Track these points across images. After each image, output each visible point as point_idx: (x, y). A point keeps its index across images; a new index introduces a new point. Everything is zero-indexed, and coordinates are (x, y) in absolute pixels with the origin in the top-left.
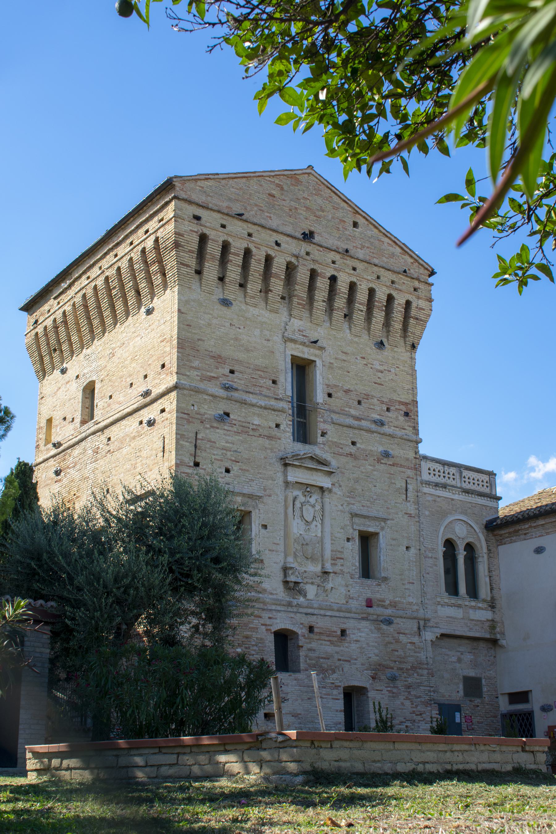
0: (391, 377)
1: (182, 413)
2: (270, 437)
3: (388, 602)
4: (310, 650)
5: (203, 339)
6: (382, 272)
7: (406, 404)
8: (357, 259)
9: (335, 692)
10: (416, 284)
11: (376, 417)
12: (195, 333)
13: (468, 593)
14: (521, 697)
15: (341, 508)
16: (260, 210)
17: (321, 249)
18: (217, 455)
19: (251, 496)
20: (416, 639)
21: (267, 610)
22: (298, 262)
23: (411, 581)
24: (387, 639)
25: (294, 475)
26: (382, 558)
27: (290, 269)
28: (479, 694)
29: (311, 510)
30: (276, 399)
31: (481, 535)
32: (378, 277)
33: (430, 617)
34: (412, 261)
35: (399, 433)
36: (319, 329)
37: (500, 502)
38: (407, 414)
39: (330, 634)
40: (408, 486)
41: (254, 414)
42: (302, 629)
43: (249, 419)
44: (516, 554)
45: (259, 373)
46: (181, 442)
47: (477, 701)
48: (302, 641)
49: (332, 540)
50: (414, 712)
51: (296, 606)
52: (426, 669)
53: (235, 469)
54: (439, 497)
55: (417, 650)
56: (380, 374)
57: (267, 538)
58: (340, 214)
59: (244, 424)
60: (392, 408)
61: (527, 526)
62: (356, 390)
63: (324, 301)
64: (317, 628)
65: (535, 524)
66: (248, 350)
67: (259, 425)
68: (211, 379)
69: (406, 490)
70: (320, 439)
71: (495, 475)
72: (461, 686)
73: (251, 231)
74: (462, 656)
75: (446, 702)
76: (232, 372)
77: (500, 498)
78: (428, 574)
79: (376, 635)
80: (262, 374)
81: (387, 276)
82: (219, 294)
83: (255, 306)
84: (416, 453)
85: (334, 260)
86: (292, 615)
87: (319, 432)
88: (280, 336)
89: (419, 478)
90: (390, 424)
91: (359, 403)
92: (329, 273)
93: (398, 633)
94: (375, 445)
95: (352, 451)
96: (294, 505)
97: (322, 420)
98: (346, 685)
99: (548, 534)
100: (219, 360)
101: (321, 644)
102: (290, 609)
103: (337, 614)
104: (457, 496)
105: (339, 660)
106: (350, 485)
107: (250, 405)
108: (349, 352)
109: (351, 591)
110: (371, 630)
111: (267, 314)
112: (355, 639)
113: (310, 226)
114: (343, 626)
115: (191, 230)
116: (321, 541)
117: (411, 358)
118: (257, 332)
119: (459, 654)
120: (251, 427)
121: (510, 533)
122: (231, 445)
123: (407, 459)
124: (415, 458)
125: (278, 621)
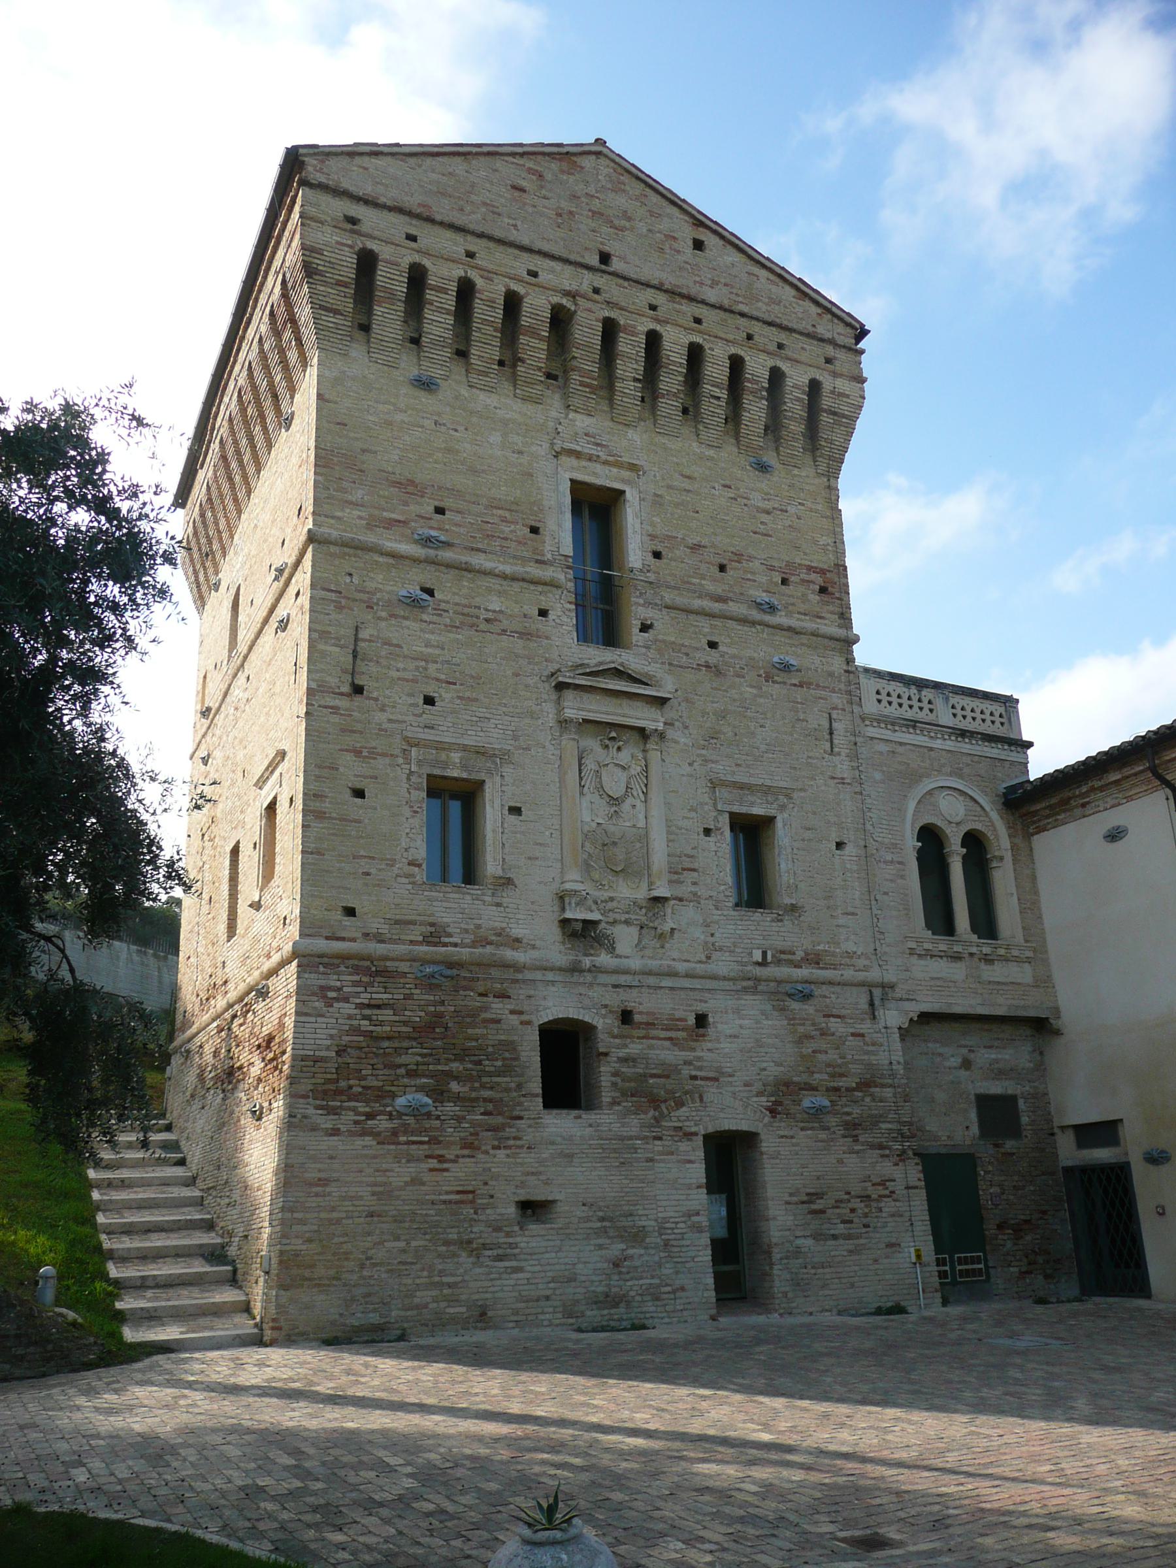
0: (788, 523)
1: (324, 589)
2: (525, 635)
3: (800, 954)
4: (624, 1060)
5: (373, 448)
6: (756, 328)
7: (822, 572)
8: (703, 302)
9: (684, 1146)
10: (830, 351)
11: (764, 597)
12: (357, 439)
13: (974, 929)
14: (1103, 1132)
15: (688, 769)
16: (494, 213)
17: (626, 284)
18: (405, 669)
19: (480, 752)
20: (865, 1027)
21: (524, 981)
22: (576, 305)
23: (850, 910)
24: (801, 1029)
25: (576, 707)
26: (783, 866)
27: (560, 320)
28: (1015, 1131)
29: (622, 777)
30: (537, 561)
31: (994, 815)
32: (750, 337)
33: (894, 980)
34: (819, 311)
35: (809, 625)
36: (631, 433)
37: (1030, 752)
38: (823, 590)
39: (673, 1024)
40: (835, 725)
41: (489, 590)
42: (604, 1016)
43: (478, 601)
44: (1067, 847)
45: (500, 512)
46: (321, 647)
47: (1010, 1145)
48: (604, 1041)
49: (668, 833)
50: (867, 1179)
51: (589, 971)
52: (891, 1086)
53: (445, 696)
54: (901, 744)
55: (871, 1048)
56: (764, 518)
57: (523, 833)
58: (664, 225)
59: (466, 610)
60: (793, 578)
61: (1084, 789)
62: (714, 546)
63: (636, 380)
64: (641, 1013)
65: (1100, 783)
66: (474, 471)
67: (501, 612)
68: (390, 524)
69: (831, 733)
70: (637, 637)
71: (1017, 701)
72: (973, 1115)
73: (472, 248)
74: (972, 1056)
75: (943, 1151)
76: (440, 511)
77: (1030, 745)
78: (886, 893)
79: (777, 1022)
80: (507, 514)
81: (766, 336)
82: (408, 366)
83: (490, 390)
84: (850, 660)
85: (654, 302)
86: (582, 990)
87: (636, 624)
88: (546, 446)
89: (856, 709)
90: (790, 608)
91: (722, 568)
92: (645, 325)
93: (824, 1016)
94: (762, 649)
95: (708, 658)
96: (580, 765)
97: (641, 601)
98: (711, 1130)
99: (1129, 799)
100: (410, 489)
101: (651, 1047)
102: (576, 977)
103: (687, 983)
104: (939, 741)
105: (694, 1078)
106: (708, 725)
107: (478, 572)
108: (696, 475)
109: (717, 935)
110: (763, 1013)
111: (518, 405)
112: (728, 1032)
113: (602, 243)
114: (701, 1008)
115: (338, 243)
116: (644, 837)
117: (829, 487)
118: (496, 438)
119: (965, 1051)
120: (484, 615)
121: (1050, 807)
122: (437, 652)
123: (831, 674)
124: (846, 671)
125: (551, 1004)
